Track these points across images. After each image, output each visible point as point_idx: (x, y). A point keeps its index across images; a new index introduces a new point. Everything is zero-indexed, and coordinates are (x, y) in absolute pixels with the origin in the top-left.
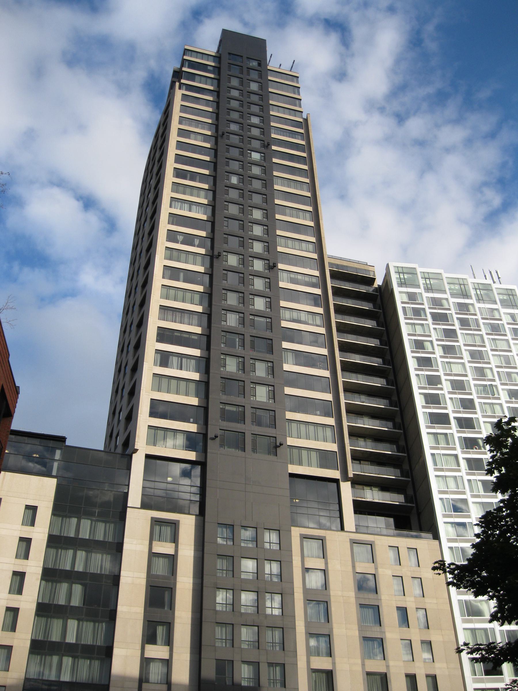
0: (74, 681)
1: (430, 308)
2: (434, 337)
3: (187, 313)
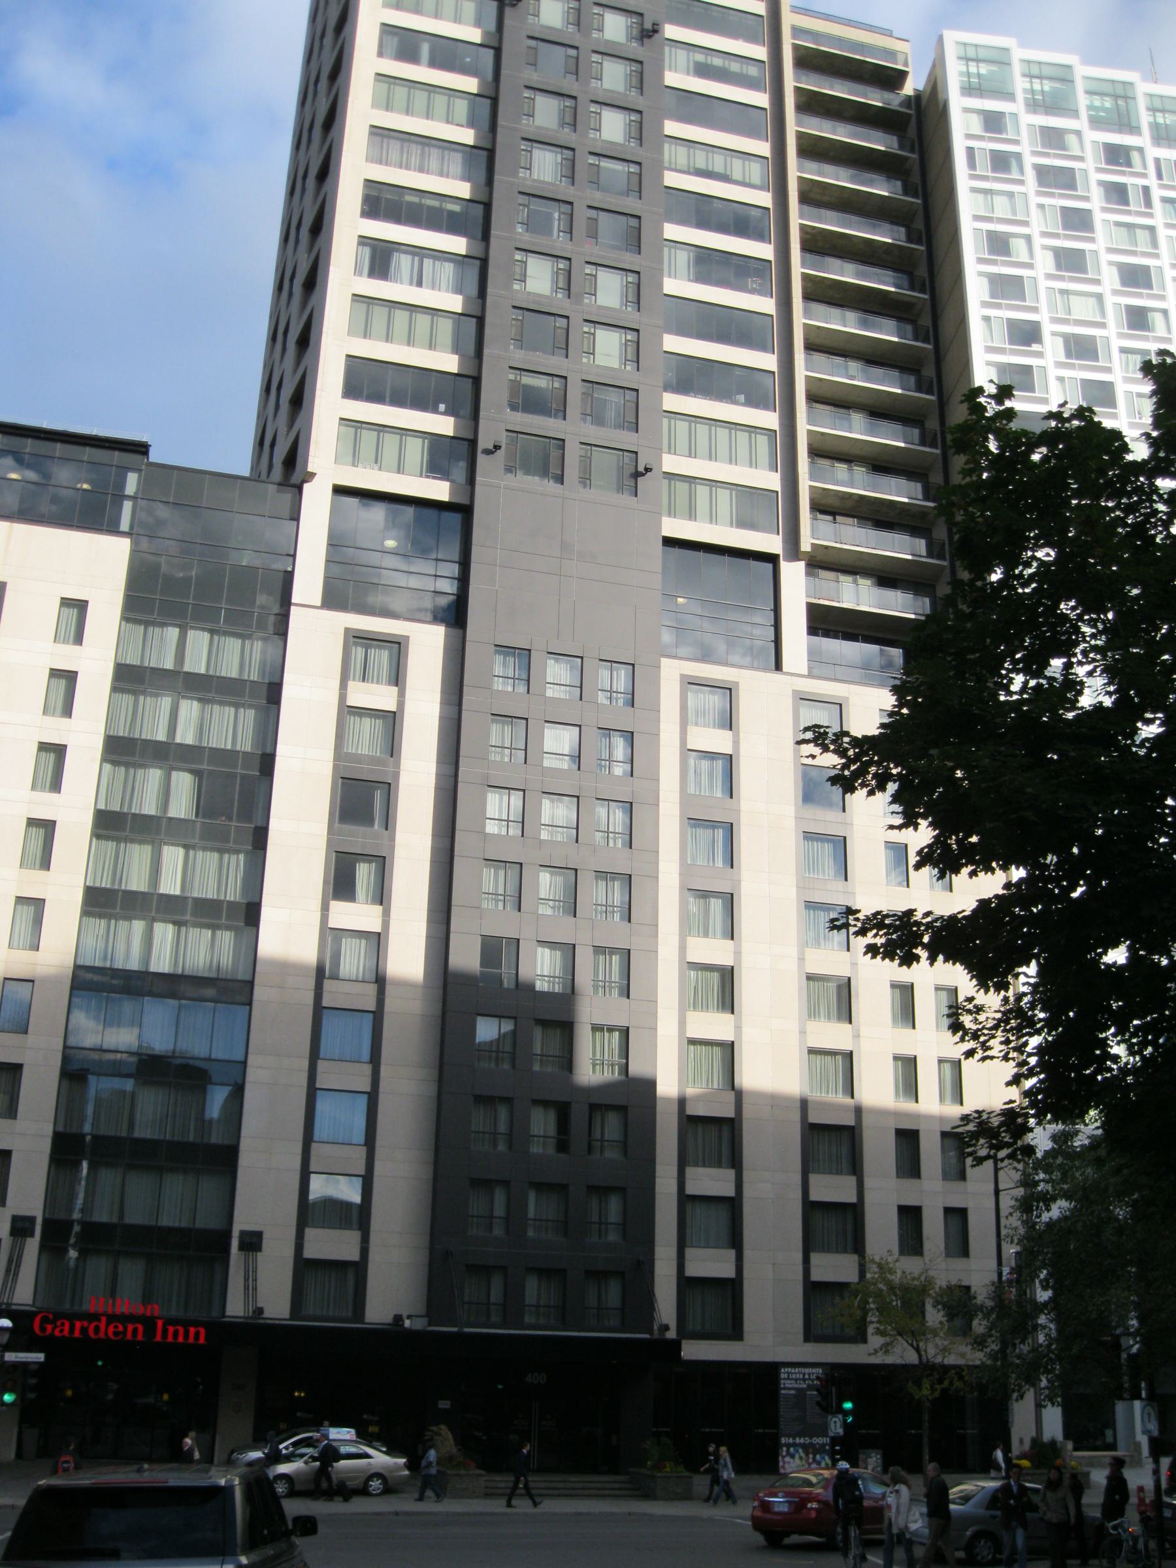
0: (180, 972)
1: (1035, 153)
2: (1036, 227)
3: (435, 146)
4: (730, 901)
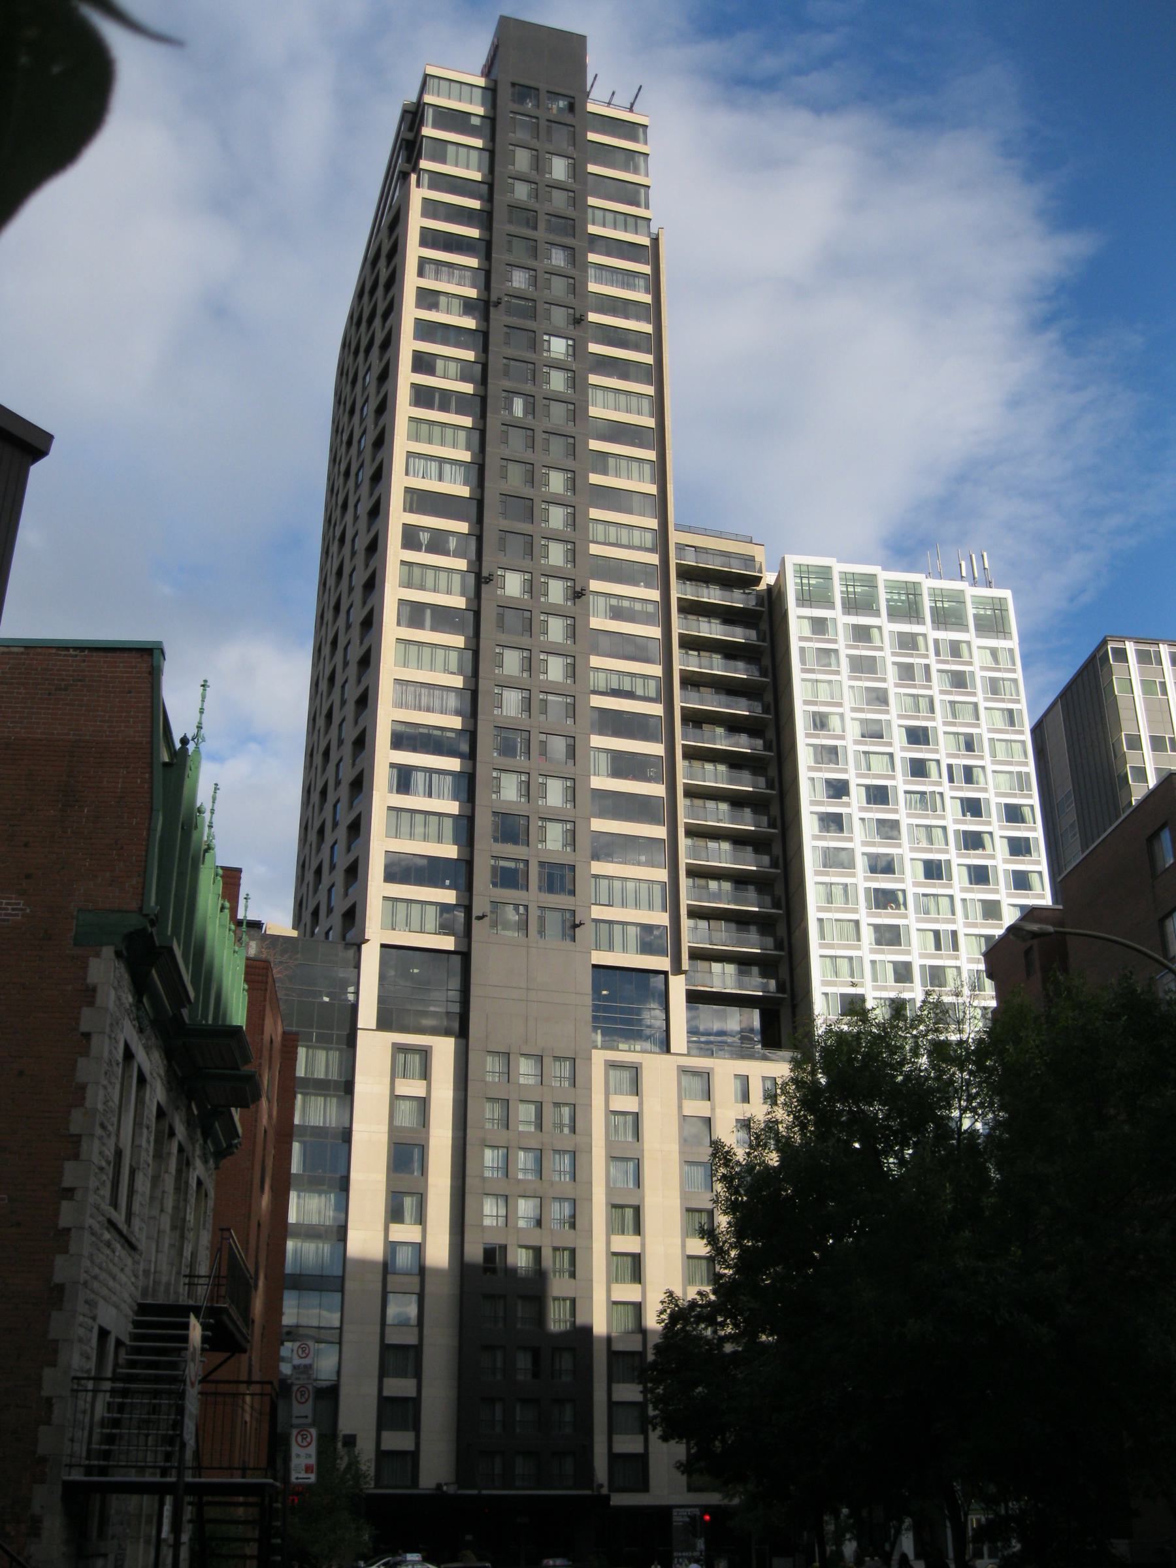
2: (846, 709)
4: (637, 1210)
